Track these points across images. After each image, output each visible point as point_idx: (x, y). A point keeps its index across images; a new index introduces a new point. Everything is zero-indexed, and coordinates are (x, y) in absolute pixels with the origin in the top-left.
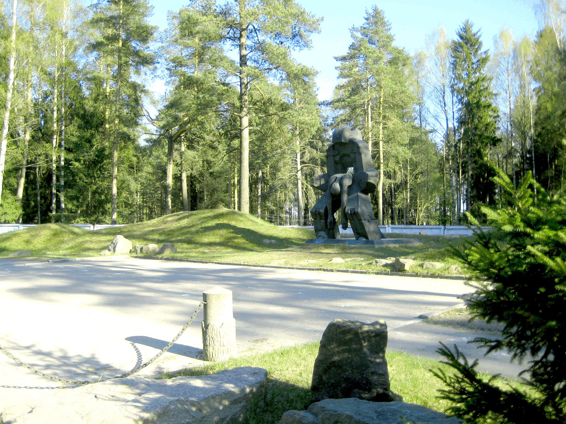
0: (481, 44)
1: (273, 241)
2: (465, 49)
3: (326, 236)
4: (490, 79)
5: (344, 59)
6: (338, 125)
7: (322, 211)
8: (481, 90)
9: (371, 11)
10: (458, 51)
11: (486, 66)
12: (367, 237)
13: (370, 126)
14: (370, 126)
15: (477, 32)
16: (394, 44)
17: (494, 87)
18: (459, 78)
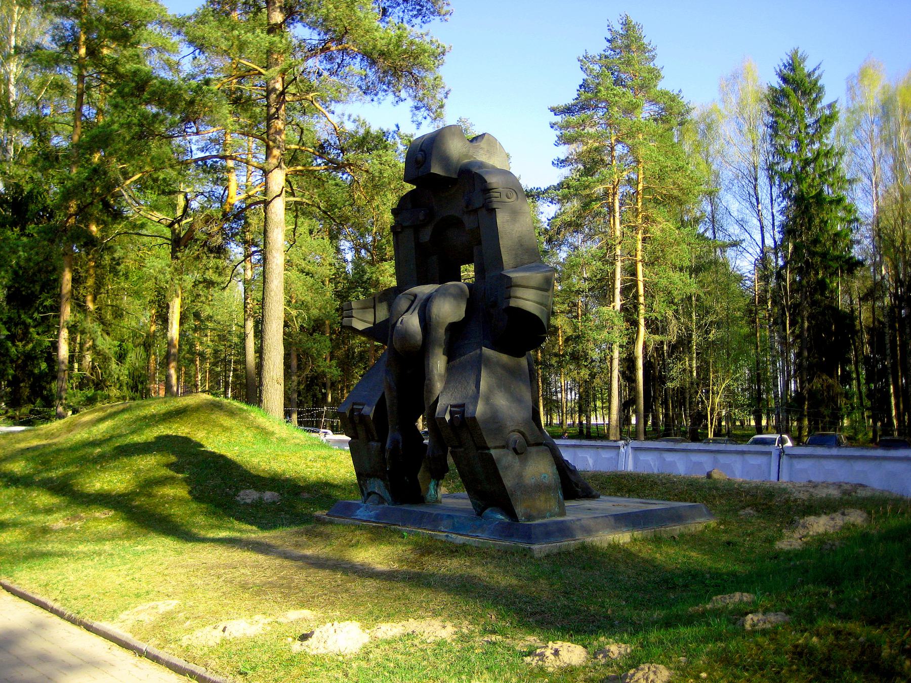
0: (821, 89)
1: (268, 495)
2: (793, 98)
3: (387, 495)
4: (840, 154)
5: (568, 110)
6: (558, 233)
7: (369, 411)
8: (824, 173)
9: (618, 27)
10: (781, 105)
11: (832, 130)
12: (510, 512)
13: (618, 233)
14: (618, 233)
15: (815, 70)
16: (662, 85)
17: (845, 168)
18: (781, 152)
